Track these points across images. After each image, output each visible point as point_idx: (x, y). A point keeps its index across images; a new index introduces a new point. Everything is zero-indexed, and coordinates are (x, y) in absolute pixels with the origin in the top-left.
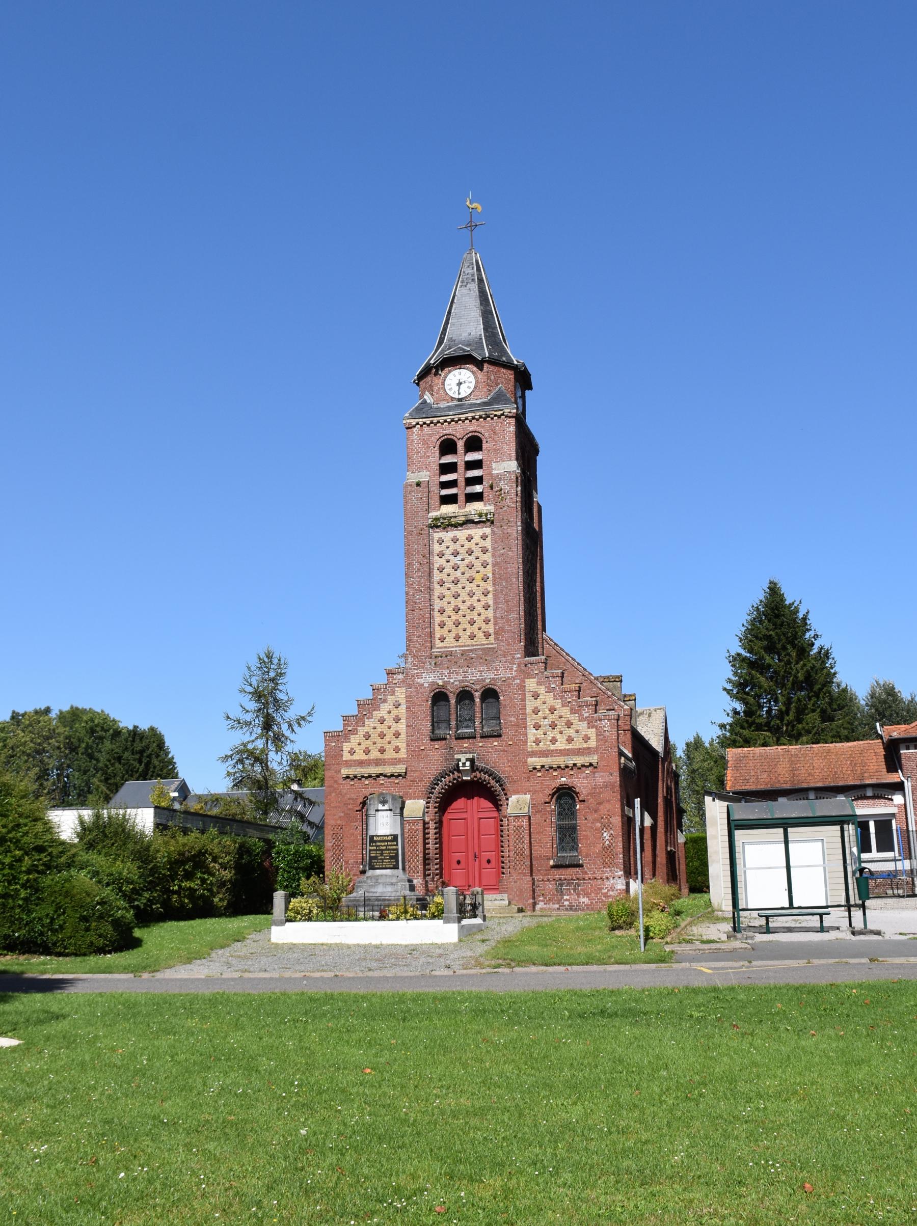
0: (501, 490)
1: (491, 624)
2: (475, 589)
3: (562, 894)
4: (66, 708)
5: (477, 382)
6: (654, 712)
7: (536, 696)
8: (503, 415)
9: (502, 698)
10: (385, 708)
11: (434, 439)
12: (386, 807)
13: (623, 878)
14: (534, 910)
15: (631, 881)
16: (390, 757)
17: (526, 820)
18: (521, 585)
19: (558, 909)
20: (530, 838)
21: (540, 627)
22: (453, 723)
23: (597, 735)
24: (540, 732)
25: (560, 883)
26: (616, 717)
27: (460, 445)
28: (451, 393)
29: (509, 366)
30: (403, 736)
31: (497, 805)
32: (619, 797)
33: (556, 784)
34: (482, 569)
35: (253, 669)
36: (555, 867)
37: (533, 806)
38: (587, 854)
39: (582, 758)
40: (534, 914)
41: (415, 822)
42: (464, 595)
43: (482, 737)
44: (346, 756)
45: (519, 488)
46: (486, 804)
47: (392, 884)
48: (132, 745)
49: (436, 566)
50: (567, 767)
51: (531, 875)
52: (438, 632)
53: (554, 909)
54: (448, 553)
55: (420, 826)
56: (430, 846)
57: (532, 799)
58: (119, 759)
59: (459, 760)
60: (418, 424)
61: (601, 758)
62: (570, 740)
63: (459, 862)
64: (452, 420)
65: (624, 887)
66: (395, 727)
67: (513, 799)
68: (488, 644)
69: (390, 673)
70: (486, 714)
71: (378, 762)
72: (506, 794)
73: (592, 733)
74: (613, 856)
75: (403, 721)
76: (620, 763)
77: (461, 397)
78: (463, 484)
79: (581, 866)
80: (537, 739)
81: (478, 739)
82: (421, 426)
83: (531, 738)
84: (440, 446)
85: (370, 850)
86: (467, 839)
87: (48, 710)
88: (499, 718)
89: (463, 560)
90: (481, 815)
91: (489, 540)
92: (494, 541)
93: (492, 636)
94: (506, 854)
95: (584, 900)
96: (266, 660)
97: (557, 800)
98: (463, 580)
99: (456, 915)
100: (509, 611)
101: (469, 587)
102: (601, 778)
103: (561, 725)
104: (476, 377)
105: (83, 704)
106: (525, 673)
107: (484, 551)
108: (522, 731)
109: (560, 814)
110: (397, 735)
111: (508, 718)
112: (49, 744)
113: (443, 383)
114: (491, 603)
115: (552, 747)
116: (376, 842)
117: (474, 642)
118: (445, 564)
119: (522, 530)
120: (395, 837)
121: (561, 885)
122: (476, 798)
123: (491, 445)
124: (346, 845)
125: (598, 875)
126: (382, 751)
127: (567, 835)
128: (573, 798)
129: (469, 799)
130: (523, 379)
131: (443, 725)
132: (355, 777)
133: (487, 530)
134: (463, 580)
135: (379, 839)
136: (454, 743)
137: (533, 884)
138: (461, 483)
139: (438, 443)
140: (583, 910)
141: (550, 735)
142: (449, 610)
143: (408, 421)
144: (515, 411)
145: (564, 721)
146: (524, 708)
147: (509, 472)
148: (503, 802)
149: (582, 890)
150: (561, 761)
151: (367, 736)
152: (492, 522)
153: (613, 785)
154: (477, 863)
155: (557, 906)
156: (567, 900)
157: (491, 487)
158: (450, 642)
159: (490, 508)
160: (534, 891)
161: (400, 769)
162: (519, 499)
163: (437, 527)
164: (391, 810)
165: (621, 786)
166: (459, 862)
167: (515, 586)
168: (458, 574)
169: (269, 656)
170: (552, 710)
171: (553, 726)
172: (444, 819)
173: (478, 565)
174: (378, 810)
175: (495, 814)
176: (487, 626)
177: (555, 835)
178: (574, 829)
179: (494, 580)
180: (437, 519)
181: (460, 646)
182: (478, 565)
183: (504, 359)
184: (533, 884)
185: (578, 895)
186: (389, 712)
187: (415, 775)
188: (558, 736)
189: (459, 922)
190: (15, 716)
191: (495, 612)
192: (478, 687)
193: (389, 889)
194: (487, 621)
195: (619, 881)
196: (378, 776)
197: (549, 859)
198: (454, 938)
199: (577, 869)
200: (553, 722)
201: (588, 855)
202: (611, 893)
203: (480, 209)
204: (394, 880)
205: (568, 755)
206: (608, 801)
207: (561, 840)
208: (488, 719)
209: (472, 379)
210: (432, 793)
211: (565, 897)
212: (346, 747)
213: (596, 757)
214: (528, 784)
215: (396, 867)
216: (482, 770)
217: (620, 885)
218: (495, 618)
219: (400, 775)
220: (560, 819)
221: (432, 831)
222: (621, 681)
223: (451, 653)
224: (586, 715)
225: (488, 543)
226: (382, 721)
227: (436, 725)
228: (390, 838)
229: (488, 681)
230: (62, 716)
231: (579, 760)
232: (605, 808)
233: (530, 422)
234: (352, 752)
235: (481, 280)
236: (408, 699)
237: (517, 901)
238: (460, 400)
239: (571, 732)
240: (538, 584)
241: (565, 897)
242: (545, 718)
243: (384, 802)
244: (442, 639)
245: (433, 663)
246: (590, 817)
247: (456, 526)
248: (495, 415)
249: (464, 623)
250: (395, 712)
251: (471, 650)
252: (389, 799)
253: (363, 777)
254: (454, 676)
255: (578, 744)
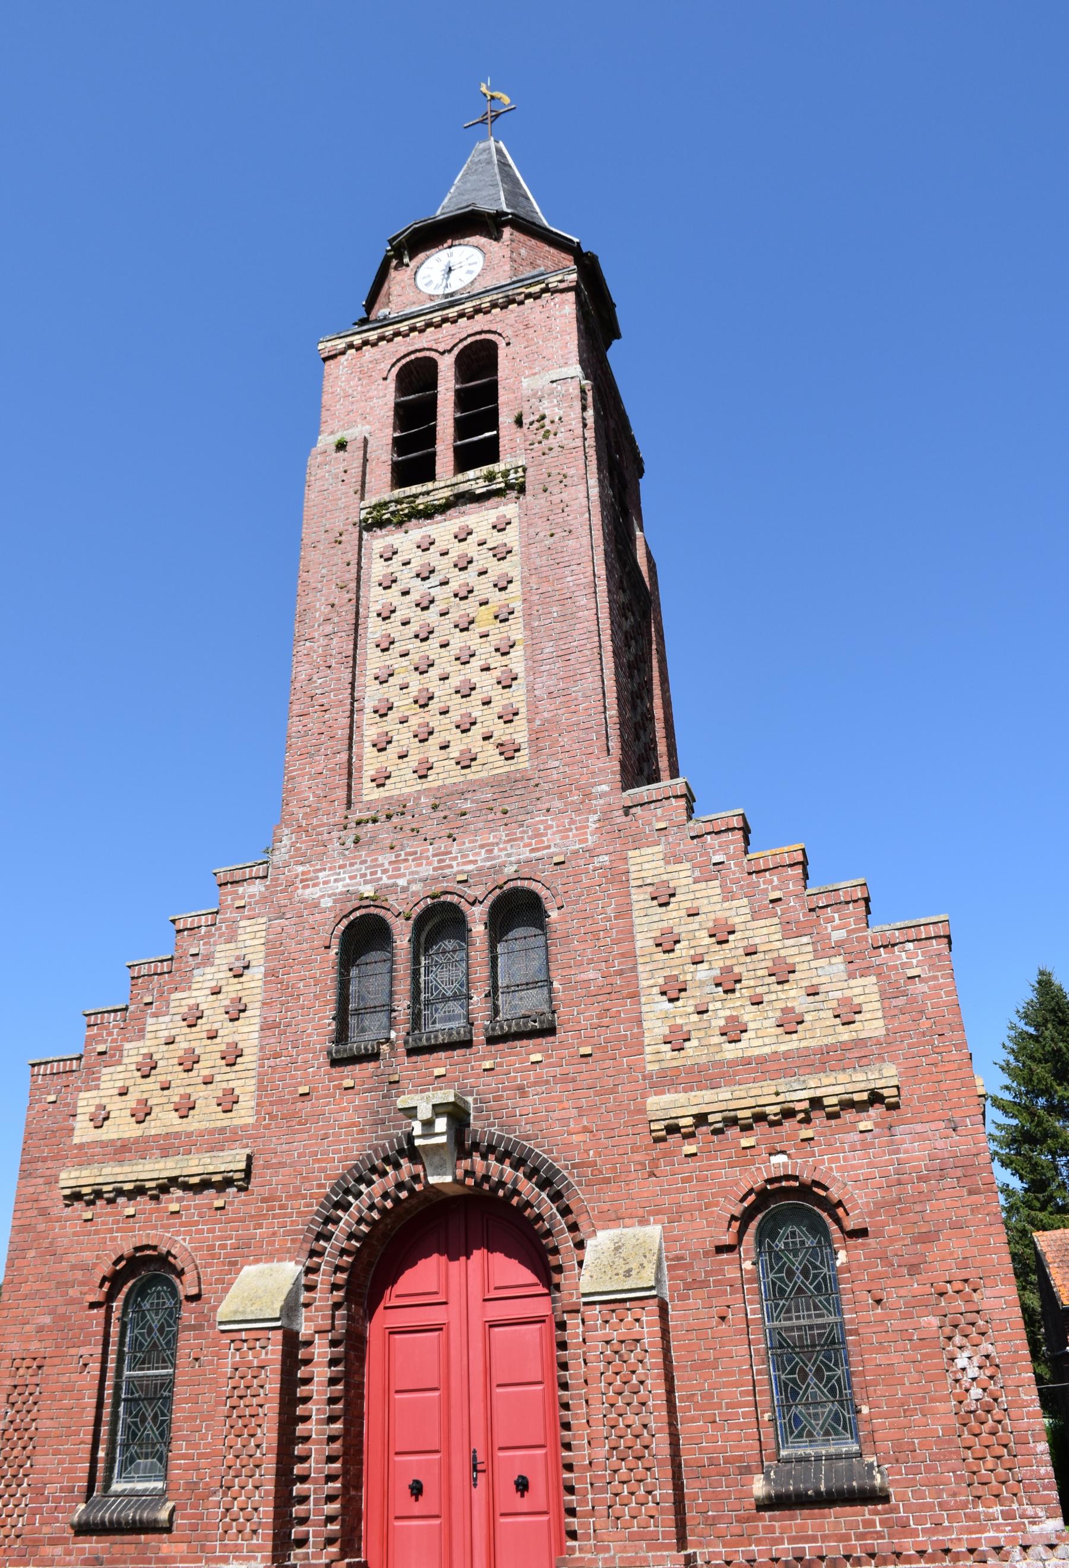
0: (543, 417)
1: (520, 722)
9: (554, 914)
17: (649, 1316)
20: (670, 1391)
23: (884, 997)
30: (249, 1060)
31: (545, 1268)
33: (755, 1177)
37: (673, 1262)
38: (899, 1448)
39: (842, 1077)
43: (491, 1040)
46: (511, 1271)
50: (788, 1114)
51: (682, 1542)
55: (274, 1352)
57: (668, 1238)
59: (411, 1112)
61: (910, 1072)
62: (790, 1023)
63: (417, 1489)
66: (229, 1033)
67: (600, 1242)
72: (574, 1227)
74: (1009, 1450)
79: (876, 1497)
80: (675, 1029)
83: (655, 1028)
84: (400, 377)
94: (580, 1456)
97: (759, 1243)
102: (917, 1143)
103: (754, 975)
106: (624, 837)
109: (777, 1292)
110: (232, 1057)
115: (731, 1052)
122: (477, 1255)
124: (44, 1425)
125: (958, 1539)
127: (811, 1370)
128: (818, 1229)
129: (453, 1257)
136: (404, 1066)
139: (395, 370)
141: (721, 1012)
145: (762, 963)
148: (566, 1257)
150: (765, 1094)
152: (522, 489)
154: (479, 1493)
158: (403, 783)
161: (232, 1161)
166: (417, 1489)
170: (721, 936)
171: (728, 983)
172: (375, 1330)
175: (541, 1307)
177: (764, 1372)
178: (831, 1346)
179: (528, 615)
188: (749, 1015)
192: (478, 892)
196: (164, 1189)
199: (866, 1512)
200: (727, 970)
201: (901, 1452)
206: (956, 1226)
207: (789, 1392)
210: (328, 1238)
216: (491, 1149)
219: (228, 1182)
221: (319, 1371)
224: (838, 935)
225: (511, 537)
227: (352, 1021)
231: (832, 1086)
232: (947, 1257)
234: (101, 1119)
236: (273, 948)
239: (794, 996)
245: (350, 843)
246: (892, 1297)
253: (120, 1192)
255: (820, 1031)
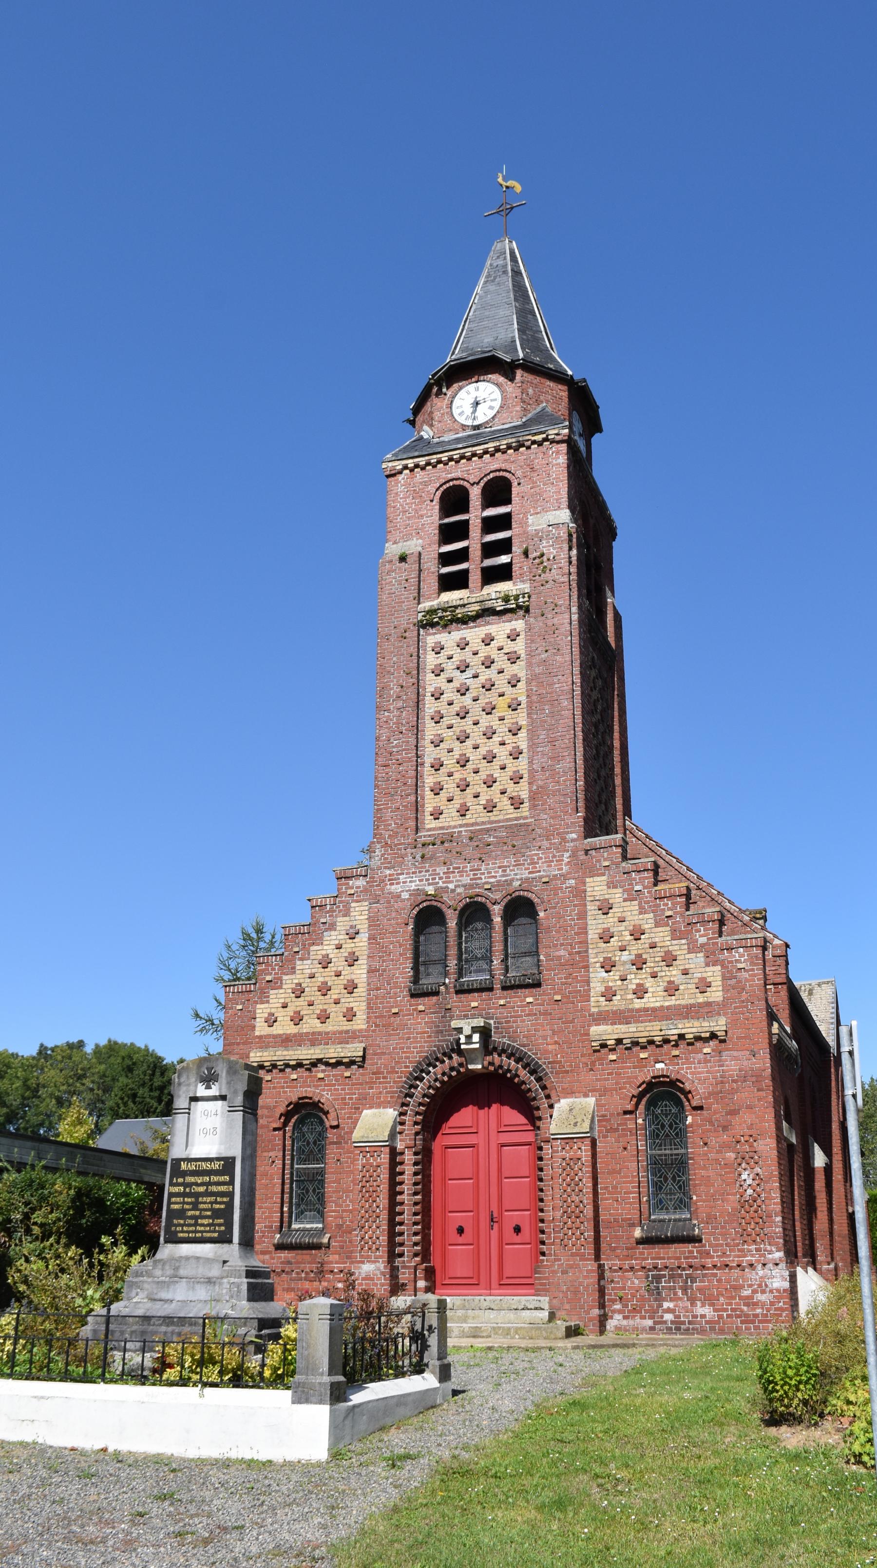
0: (542, 555)
1: (524, 783)
2: (496, 724)
3: (660, 1299)
4: (103, 1042)
5: (504, 398)
6: (817, 988)
7: (606, 909)
8: (546, 439)
9: (542, 914)
10: (332, 938)
11: (431, 488)
12: (214, 1091)
13: (783, 1265)
14: (602, 1329)
15: (799, 1270)
16: (336, 1028)
17: (586, 1147)
18: (578, 712)
19: (652, 1329)
21: (619, 806)
22: (452, 963)
23: (724, 978)
24: (615, 975)
25: (654, 1274)
26: (760, 942)
27: (475, 493)
28: (462, 420)
29: (558, 376)
30: (362, 990)
32: (771, 1099)
34: (508, 690)
35: (235, 947)
36: (645, 1241)
38: (709, 1216)
39: (696, 1023)
40: (603, 1340)
41: (374, 1150)
42: (476, 736)
43: (504, 988)
44: (261, 1028)
45: (574, 552)
46: (512, 1116)
47: (210, 1281)
48: (151, 1080)
49: (430, 689)
50: (666, 1041)
51: (597, 1257)
52: (430, 802)
53: (644, 1329)
54: (450, 666)
55: (385, 1158)
56: (405, 1197)
57: (598, 1104)
58: (134, 1096)
59: (460, 1030)
60: (406, 467)
61: (733, 1023)
62: (672, 989)
63: (461, 1231)
64: (462, 457)
65: (787, 1285)
67: (562, 1105)
68: (517, 819)
69: (343, 877)
70: (516, 947)
71: (314, 1039)
72: (548, 1097)
73: (714, 974)
74: (763, 1219)
75: (363, 962)
76: (770, 1034)
77: (476, 423)
78: (478, 553)
79: (697, 1240)
80: (608, 988)
81: (498, 992)
82: (412, 470)
83: (597, 987)
84: (442, 499)
85: (171, 1195)
86: (477, 1186)
87: (81, 1044)
88: (537, 954)
89: (476, 676)
90: (505, 1138)
91: (521, 641)
92: (530, 641)
93: (526, 805)
94: (548, 1215)
95: (705, 1311)
96: (254, 935)
97: (647, 1108)
98: (476, 711)
99: (326, 1379)
100: (556, 758)
101: (460, 678)
102: (734, 1062)
103: (653, 959)
104: (503, 392)
105: (124, 1037)
107: (513, 658)
108: (580, 974)
109: (655, 1135)
110: (351, 987)
111: (554, 951)
112: (83, 1084)
113: (450, 405)
114: (524, 746)
115: (638, 1004)
116: (184, 1174)
117: (493, 816)
118: (445, 686)
119: (580, 621)
120: (228, 1163)
121: (658, 1279)
122: (494, 1107)
123: (526, 488)
126: (324, 1017)
127: (669, 1176)
128: (679, 1104)
129: (481, 1107)
130: (584, 407)
131: (435, 970)
132: (274, 1066)
133: (519, 624)
134: (476, 711)
135: (192, 1167)
136: (454, 1000)
137: (601, 1277)
138: (475, 552)
139: (439, 494)
140: (702, 1331)
141: (634, 981)
142: (450, 762)
143: (390, 464)
144: (566, 431)
145: (659, 953)
146: (584, 930)
147: (556, 525)
149: (700, 1289)
150: (654, 1029)
151: (299, 992)
152: (527, 610)
153: (758, 1077)
154: (495, 1233)
155: (649, 1323)
156: (669, 1311)
157: (526, 553)
158: (450, 819)
159: (526, 587)
160: (602, 1291)
161: (354, 1050)
162: (574, 570)
163: (433, 625)
164: (223, 1098)
165: (773, 1079)
166: (461, 1231)
167: (568, 713)
168: (467, 700)
169: (259, 931)
170: (637, 934)
171: (639, 963)
172: (436, 1146)
173: (501, 683)
174: (195, 1099)
175: (529, 1137)
176: (517, 788)
178: (681, 1165)
180: (432, 612)
181: (467, 825)
182: (501, 683)
183: (551, 366)
184: (601, 1277)
185: (693, 1301)
186: (339, 947)
187: (381, 1062)
188: (649, 983)
189: (337, 1395)
190: (43, 1050)
191: (531, 762)
192: (497, 896)
193: (202, 1293)
194: (516, 779)
195: (776, 1272)
196: (315, 1064)
197: (633, 1225)
198: (317, 1449)
200: (639, 956)
201: (710, 1219)
202: (760, 1297)
203: (518, 188)
204: (215, 1271)
205: (668, 1018)
206: (749, 1107)
207: (658, 1187)
208: (517, 956)
209: (497, 394)
210: (411, 1096)
211: (666, 1305)
212: (262, 1011)
213: (722, 1021)
214: (591, 1076)
215: (225, 1239)
216: (504, 1051)
217: (779, 1281)
218: (532, 772)
219: (352, 1062)
220: (654, 1146)
221: (408, 1169)
222: (765, 918)
223: (451, 838)
225: (519, 647)
226: (325, 963)
227: (422, 969)
228: (216, 1166)
229: (516, 884)
230: (97, 1050)
231: (691, 1028)
232: (742, 1123)
233: (600, 473)
234: (271, 1021)
235: (517, 273)
236: (373, 921)
237: (569, 1313)
238: (477, 427)
239: (674, 974)
240: (616, 735)
241: (666, 1305)
242: (622, 949)
243: (209, 1079)
244: (437, 814)
245: (418, 857)
246: (713, 1141)
247: (464, 621)
248: (534, 442)
249: (477, 784)
250: (349, 946)
251: (488, 830)
252: (221, 1070)
253: (287, 1066)
254: (455, 877)
255: (688, 996)
